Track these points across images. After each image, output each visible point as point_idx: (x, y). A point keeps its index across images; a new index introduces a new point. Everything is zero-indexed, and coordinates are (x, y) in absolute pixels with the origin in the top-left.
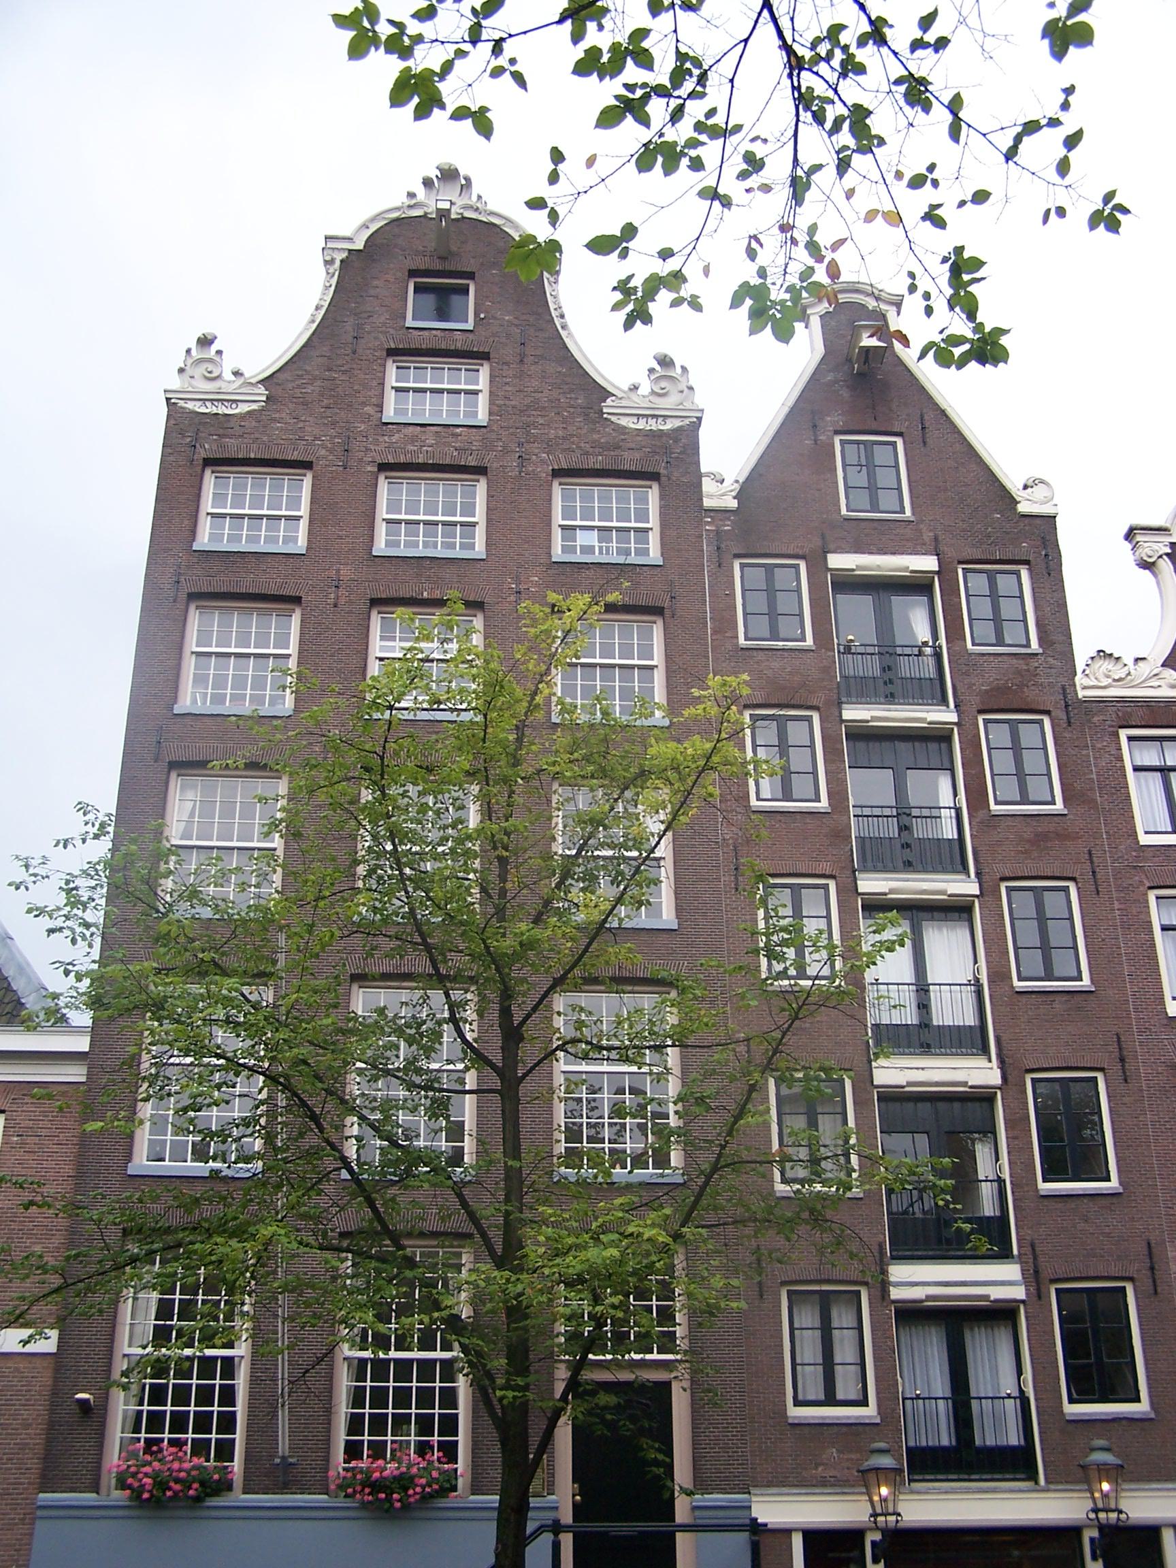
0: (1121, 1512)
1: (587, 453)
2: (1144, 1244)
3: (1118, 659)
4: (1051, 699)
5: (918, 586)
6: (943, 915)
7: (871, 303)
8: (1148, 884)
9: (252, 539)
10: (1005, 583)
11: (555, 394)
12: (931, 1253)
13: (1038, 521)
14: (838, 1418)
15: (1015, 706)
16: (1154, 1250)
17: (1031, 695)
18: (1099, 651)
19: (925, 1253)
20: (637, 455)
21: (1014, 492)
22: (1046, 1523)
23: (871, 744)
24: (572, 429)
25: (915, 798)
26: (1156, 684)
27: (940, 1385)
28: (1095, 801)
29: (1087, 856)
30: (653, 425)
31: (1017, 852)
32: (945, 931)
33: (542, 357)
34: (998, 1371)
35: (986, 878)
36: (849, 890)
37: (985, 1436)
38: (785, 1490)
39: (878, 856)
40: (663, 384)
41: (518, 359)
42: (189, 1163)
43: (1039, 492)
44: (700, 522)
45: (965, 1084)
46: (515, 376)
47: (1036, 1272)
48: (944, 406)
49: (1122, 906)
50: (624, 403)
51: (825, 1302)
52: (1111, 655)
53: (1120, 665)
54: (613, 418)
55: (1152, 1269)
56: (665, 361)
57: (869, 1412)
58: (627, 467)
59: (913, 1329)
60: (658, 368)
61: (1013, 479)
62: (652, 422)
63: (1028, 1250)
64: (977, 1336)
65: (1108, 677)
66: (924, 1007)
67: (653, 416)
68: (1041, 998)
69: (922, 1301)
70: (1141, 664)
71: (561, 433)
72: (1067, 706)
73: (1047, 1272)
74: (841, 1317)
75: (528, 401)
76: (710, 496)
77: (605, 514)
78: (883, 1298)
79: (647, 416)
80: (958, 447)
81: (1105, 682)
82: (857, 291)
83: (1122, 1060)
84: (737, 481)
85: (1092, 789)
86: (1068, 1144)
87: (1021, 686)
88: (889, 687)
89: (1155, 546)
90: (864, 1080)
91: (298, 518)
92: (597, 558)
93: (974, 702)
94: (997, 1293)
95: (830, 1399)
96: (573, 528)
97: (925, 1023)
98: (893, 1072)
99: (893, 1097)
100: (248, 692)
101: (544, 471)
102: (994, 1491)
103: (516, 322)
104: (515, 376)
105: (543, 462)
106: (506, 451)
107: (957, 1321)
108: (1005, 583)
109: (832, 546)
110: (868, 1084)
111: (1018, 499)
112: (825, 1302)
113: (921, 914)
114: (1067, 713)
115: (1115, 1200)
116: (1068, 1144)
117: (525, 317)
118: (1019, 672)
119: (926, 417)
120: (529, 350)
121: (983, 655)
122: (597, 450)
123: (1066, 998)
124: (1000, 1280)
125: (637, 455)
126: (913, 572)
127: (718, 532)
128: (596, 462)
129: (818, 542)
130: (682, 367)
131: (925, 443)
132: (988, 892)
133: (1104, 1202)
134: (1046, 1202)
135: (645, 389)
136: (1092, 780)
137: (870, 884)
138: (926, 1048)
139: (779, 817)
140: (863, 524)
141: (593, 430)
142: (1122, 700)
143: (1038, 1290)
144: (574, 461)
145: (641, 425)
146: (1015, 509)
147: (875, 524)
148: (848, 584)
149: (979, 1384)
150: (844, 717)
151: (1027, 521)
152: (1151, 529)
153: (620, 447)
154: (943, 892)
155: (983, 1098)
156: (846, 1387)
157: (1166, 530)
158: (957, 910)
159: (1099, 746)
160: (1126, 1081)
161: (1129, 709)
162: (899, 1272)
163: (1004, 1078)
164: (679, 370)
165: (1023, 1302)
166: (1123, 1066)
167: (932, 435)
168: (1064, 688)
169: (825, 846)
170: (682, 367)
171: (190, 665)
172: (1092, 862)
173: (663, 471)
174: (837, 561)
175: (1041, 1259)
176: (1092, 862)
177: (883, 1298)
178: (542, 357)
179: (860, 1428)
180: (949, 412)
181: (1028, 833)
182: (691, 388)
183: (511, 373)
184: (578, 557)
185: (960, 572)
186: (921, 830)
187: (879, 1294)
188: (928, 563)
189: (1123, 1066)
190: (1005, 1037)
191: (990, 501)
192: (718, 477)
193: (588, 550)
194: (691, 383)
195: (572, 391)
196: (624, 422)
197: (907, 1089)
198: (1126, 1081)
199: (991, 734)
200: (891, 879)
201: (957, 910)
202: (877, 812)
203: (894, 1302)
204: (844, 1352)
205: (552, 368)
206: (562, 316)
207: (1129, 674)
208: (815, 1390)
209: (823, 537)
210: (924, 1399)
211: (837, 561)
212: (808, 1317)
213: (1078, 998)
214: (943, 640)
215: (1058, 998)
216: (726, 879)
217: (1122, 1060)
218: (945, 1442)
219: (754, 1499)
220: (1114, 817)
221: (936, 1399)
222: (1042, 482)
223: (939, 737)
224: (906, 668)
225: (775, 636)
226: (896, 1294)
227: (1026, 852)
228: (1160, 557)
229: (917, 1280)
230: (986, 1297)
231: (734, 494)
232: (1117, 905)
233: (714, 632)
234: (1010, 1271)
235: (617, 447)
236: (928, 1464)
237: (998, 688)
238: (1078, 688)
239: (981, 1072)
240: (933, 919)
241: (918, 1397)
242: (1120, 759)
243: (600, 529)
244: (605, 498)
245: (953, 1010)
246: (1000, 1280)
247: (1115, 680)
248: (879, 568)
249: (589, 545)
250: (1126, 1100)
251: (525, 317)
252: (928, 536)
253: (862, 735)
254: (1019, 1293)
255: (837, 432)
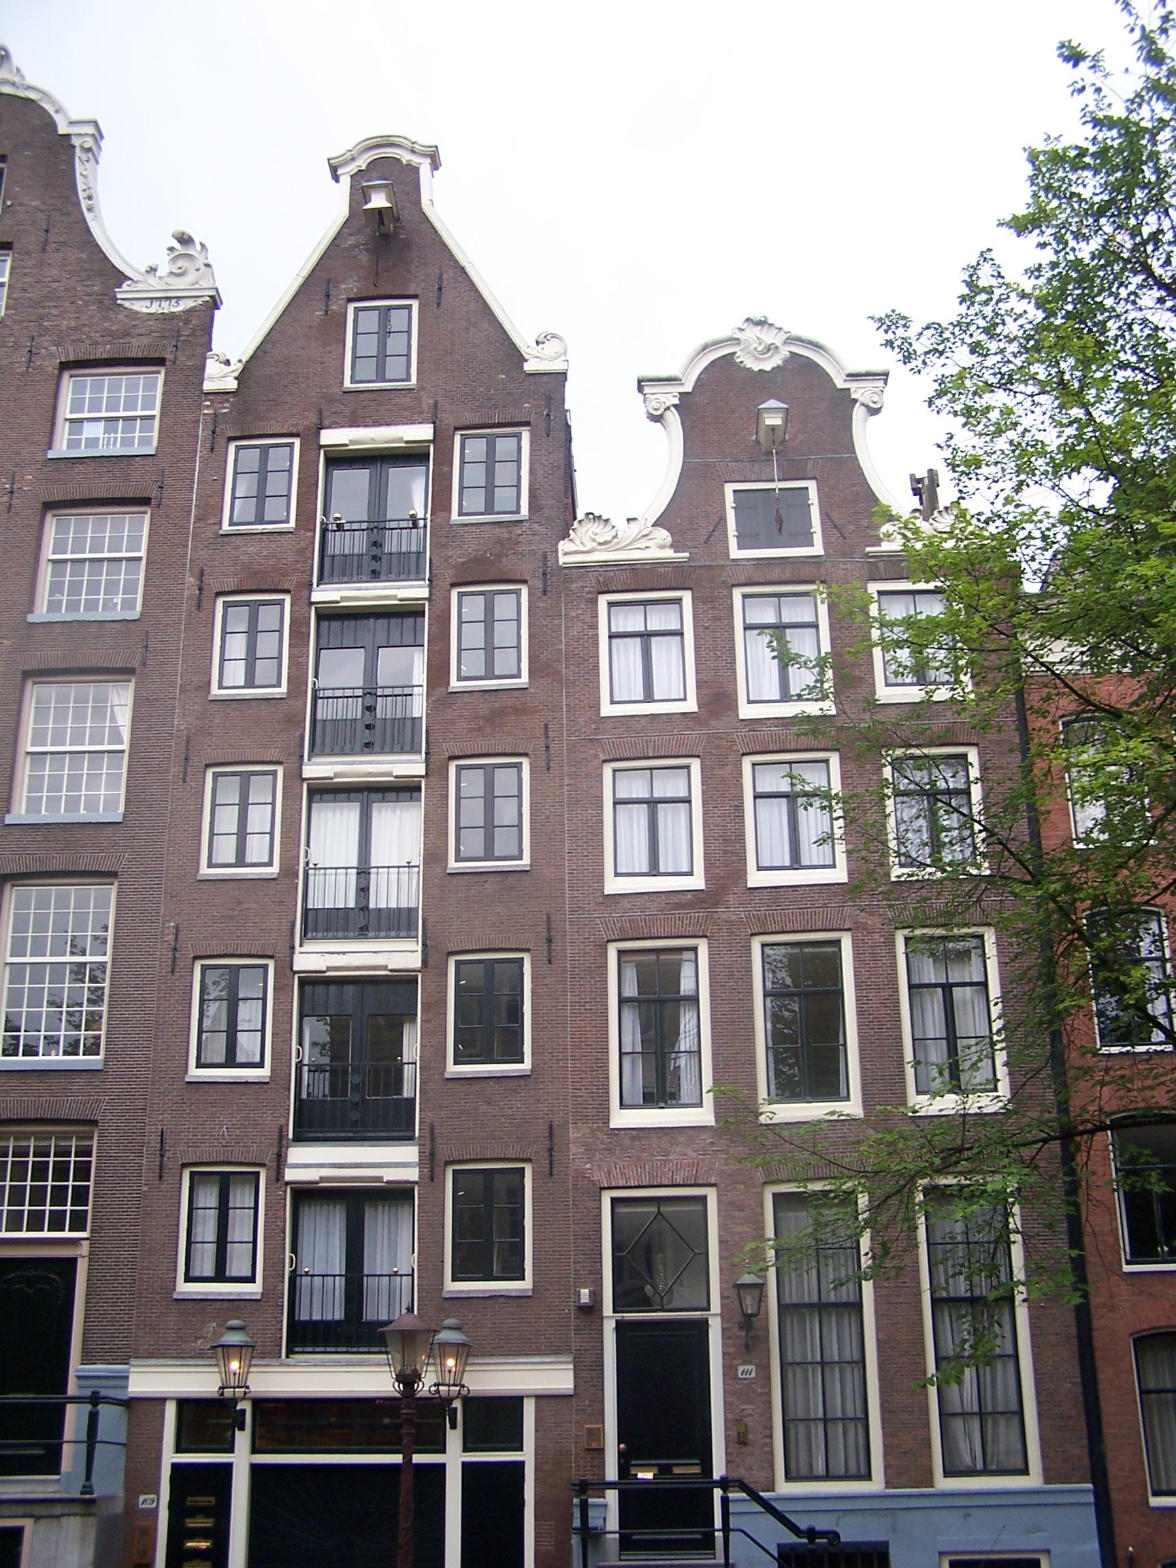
0: (463, 1386)
1: (96, 343)
2: (546, 1128)
3: (607, 521)
4: (528, 567)
5: (412, 456)
6: (380, 795)
7: (405, 157)
8: (603, 757)
9: (127, 442)
10: (504, 447)
11: (72, 283)
12: (383, 1134)
13: (545, 379)
14: (220, 1294)
15: (489, 578)
16: (555, 1132)
17: (509, 564)
18: (587, 514)
19: (334, 1135)
20: (145, 341)
21: (523, 349)
22: (189, 1395)
23: (346, 623)
24: (84, 318)
25: (384, 677)
26: (642, 545)
27: (337, 1265)
28: (559, 672)
29: (542, 731)
30: (166, 308)
31: (474, 726)
32: (398, 812)
33: (64, 243)
34: (395, 1250)
35: (432, 758)
36: (295, 776)
37: (375, 1310)
38: (162, 1361)
39: (331, 738)
40: (180, 263)
41: (40, 248)
42: (40, 1057)
43: (551, 348)
44: (200, 407)
45: (385, 968)
46: (35, 266)
47: (432, 1154)
48: (463, 263)
49: (573, 782)
50: (140, 287)
51: (225, 1183)
52: (600, 517)
53: (609, 528)
54: (127, 304)
55: (551, 1150)
56: (185, 240)
57: (255, 1289)
58: (133, 355)
59: (331, 1208)
60: (177, 246)
61: (523, 334)
62: (165, 304)
63: (427, 1132)
64: (380, 1216)
65: (594, 540)
66: (363, 890)
67: (167, 298)
68: (473, 879)
69: (317, 1183)
70: (632, 524)
71: (73, 324)
72: (545, 574)
73: (443, 1154)
74: (240, 1197)
75: (45, 291)
76: (212, 379)
77: (113, 406)
78: (278, 1180)
79: (160, 299)
80: (473, 306)
81: (590, 545)
82: (392, 145)
83: (550, 941)
84: (240, 361)
85: (559, 661)
86: (489, 1023)
87: (499, 556)
88: (376, 565)
89: (662, 398)
90: (285, 967)
91: (152, 417)
92: (101, 451)
93: (449, 575)
94: (390, 1175)
95: (220, 1275)
96: (81, 421)
97: (363, 908)
98: (313, 957)
99: (311, 981)
100: (84, 597)
101: (51, 366)
102: (361, 1364)
103: (43, 208)
104: (35, 266)
105: (52, 355)
106: (17, 346)
107: (357, 1201)
108: (504, 447)
109: (327, 422)
110: (288, 971)
111: (526, 357)
112: (225, 1183)
113: (373, 796)
114: (545, 581)
115: (522, 1083)
116: (489, 1023)
117: (52, 201)
118: (500, 542)
119: (445, 276)
120: (52, 237)
121: (466, 525)
122: (107, 338)
123: (499, 878)
124: (395, 1161)
125: (145, 341)
126: (407, 442)
127: (215, 415)
128: (103, 352)
129: (313, 418)
130: (202, 245)
131: (438, 305)
132: (435, 770)
133: (514, 1083)
134: (450, 1084)
135: (163, 270)
136: (559, 651)
137: (317, 769)
138: (363, 932)
139: (234, 705)
140: (362, 396)
141: (106, 318)
142: (604, 565)
143: (432, 1171)
144: (84, 352)
145: (155, 308)
146: (522, 368)
147: (375, 395)
148: (341, 459)
149: (376, 1260)
150: (313, 600)
151: (532, 379)
152: (660, 380)
153: (128, 334)
154: (389, 774)
155: (403, 982)
156: (238, 1264)
157: (675, 379)
158: (404, 790)
159: (573, 614)
160: (550, 962)
161: (612, 574)
162: (297, 1154)
163: (425, 962)
164: (198, 247)
165: (416, 1183)
166: (549, 946)
167: (448, 293)
168: (545, 556)
169: (280, 731)
170: (202, 245)
171: (46, 575)
172: (547, 737)
173: (169, 356)
174: (330, 437)
175: (439, 1141)
176: (547, 737)
177: (278, 1180)
178: (64, 243)
179: (242, 1304)
180: (469, 269)
181: (484, 710)
182: (208, 265)
183: (31, 263)
184: (83, 452)
185: (457, 439)
186: (384, 709)
187: (274, 1174)
188: (423, 432)
189: (549, 946)
190: (431, 920)
191: (497, 361)
192: (222, 359)
193: (92, 442)
194: (210, 261)
195: (89, 278)
196: (137, 307)
197: (328, 974)
198: (550, 962)
199: (465, 607)
200: (337, 763)
201: (404, 790)
202: (339, 693)
203: (287, 1183)
204: (239, 1230)
205: (74, 254)
206: (90, 198)
207: (616, 536)
208: (206, 1266)
209: (320, 412)
210: (312, 1276)
211: (330, 437)
212: (208, 1197)
213: (511, 878)
214: (428, 515)
215: (491, 879)
216: (175, 770)
217: (550, 941)
218: (337, 1317)
219: (132, 1370)
220: (577, 688)
221: (335, 1276)
222: (554, 336)
223: (409, 612)
224: (394, 543)
225: (260, 520)
226: (290, 1175)
227: (480, 729)
228: (668, 409)
229: (311, 1162)
230: (380, 1179)
231: (236, 374)
232: (566, 781)
233: (198, 519)
234: (408, 1153)
235: (127, 334)
236: (309, 1337)
237: (475, 560)
238: (560, 554)
239: (401, 955)
240: (383, 800)
241: (396, 1274)
242: (595, 626)
243: (107, 419)
244: (132, 387)
245: (390, 892)
246: (395, 1161)
247: (600, 544)
248: (373, 441)
249: (97, 439)
250: (548, 981)
251: (52, 201)
252: (427, 402)
253: (330, 615)
254: (412, 1175)
255: (350, 300)
